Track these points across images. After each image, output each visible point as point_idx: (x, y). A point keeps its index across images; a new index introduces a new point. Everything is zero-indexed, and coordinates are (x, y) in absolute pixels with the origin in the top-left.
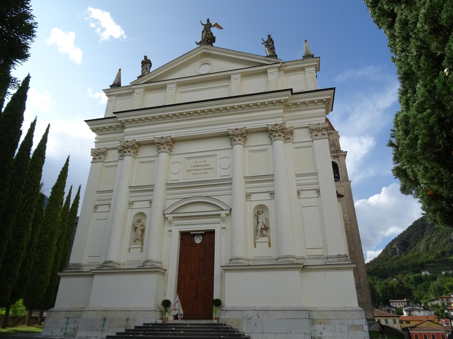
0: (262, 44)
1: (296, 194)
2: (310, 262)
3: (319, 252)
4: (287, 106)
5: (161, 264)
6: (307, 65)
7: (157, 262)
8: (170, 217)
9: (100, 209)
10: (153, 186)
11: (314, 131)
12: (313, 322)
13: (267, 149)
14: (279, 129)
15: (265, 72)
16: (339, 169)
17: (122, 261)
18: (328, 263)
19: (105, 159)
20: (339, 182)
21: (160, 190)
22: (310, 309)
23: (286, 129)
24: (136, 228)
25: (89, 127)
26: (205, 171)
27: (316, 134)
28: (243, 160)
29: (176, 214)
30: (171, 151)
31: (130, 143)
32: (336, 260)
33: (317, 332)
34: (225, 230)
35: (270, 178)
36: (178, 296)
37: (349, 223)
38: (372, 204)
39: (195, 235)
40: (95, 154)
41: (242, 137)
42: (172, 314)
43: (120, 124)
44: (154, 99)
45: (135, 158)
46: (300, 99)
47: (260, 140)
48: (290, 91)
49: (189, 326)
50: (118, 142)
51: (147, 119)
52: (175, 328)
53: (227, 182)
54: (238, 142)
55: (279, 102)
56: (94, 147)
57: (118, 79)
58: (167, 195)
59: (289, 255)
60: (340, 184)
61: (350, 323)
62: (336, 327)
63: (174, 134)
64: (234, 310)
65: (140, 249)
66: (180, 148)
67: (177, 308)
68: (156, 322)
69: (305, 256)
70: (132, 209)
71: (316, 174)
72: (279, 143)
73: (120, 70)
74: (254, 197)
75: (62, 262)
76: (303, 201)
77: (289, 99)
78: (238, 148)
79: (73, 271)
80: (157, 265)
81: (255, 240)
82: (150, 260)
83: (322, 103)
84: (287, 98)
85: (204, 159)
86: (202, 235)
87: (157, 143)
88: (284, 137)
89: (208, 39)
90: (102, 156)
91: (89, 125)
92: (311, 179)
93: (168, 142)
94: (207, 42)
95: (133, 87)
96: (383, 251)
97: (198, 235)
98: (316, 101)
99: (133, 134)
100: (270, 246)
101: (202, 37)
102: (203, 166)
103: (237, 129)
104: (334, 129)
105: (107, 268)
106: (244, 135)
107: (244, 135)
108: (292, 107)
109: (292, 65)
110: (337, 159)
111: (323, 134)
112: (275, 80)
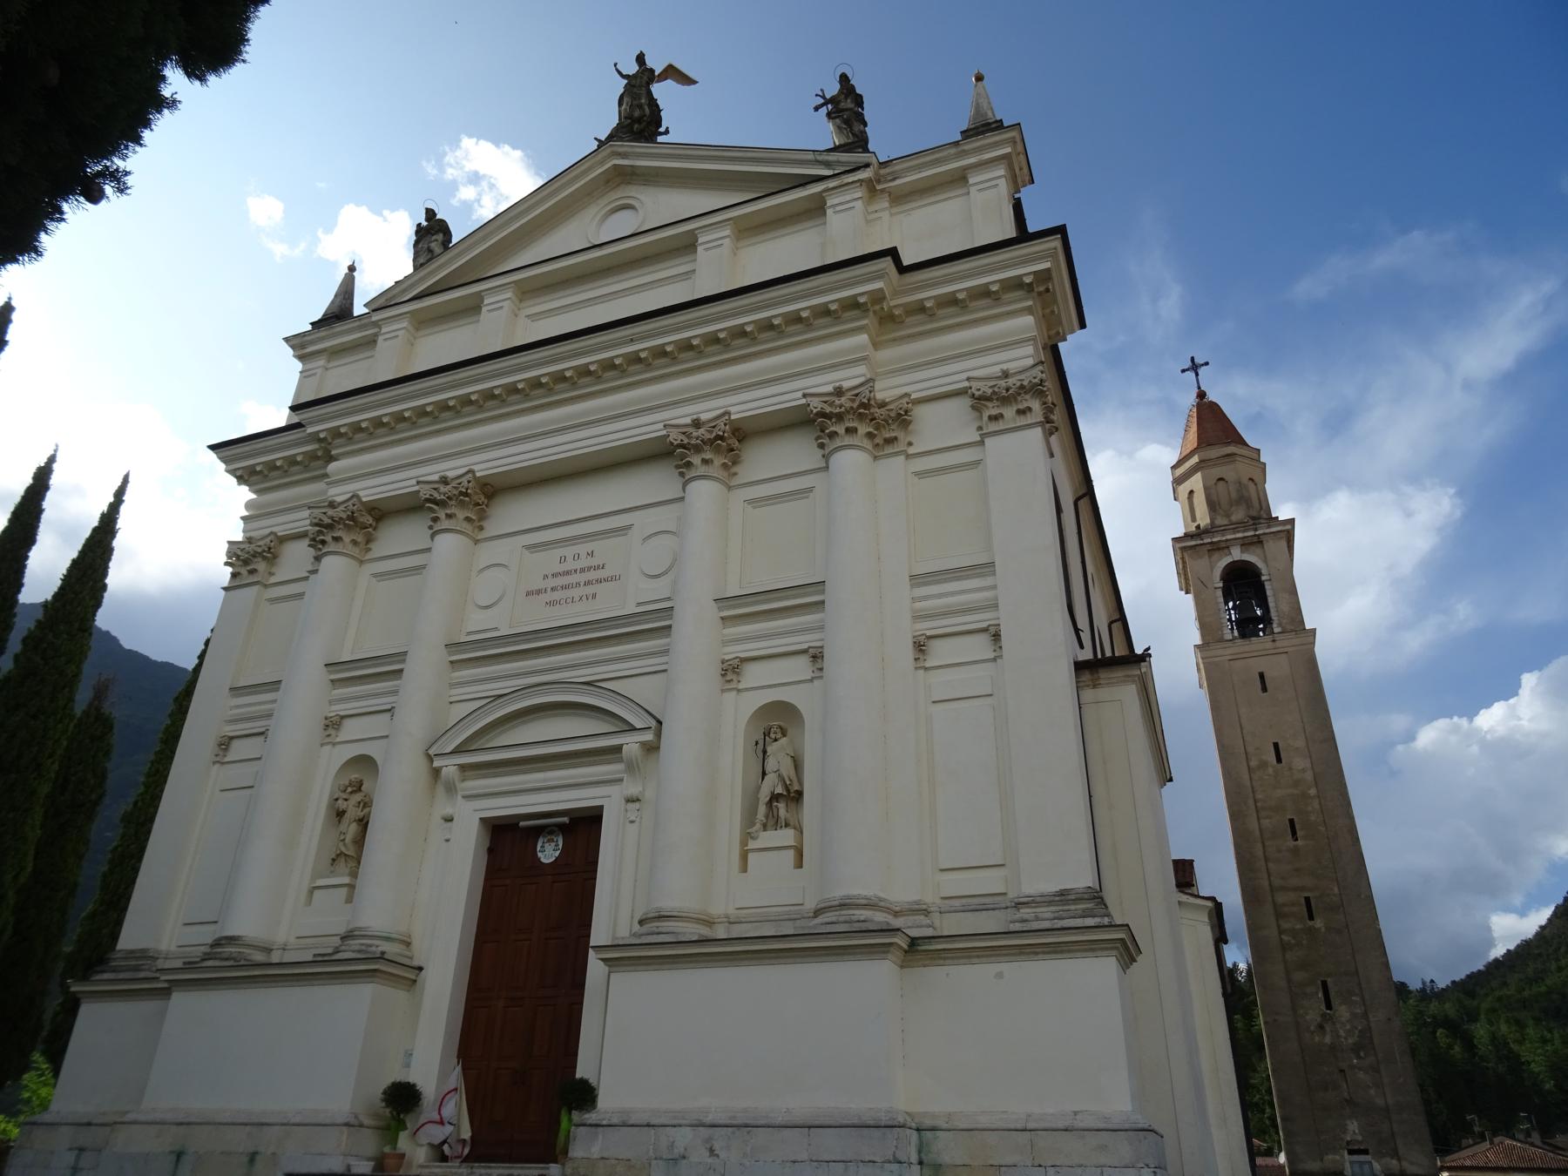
0: (817, 109)
1: (909, 652)
2: (949, 925)
3: (988, 883)
4: (888, 320)
6: (972, 160)
7: (388, 939)
8: (449, 767)
9: (941, 652)
10: (401, 656)
11: (991, 402)
13: (811, 489)
14: (848, 405)
16: (1268, 586)
17: (282, 935)
18: (1013, 927)
19: (271, 574)
20: (1269, 638)
21: (425, 669)
22: (928, 1123)
23: (883, 405)
24: (340, 814)
25: (223, 466)
26: (590, 590)
27: (994, 412)
29: (474, 753)
30: (481, 528)
31: (342, 508)
32: (1046, 911)
34: (637, 805)
35: (807, 598)
36: (459, 1068)
37: (1313, 792)
39: (538, 831)
40: (238, 557)
41: (718, 450)
42: (424, 1141)
45: (361, 562)
46: (931, 287)
47: (786, 456)
48: (906, 263)
50: (306, 513)
51: (400, 418)
53: (654, 624)
54: (702, 470)
55: (853, 304)
56: (239, 537)
58: (452, 686)
59: (854, 897)
60: (1269, 645)
63: (486, 465)
64: (625, 1125)
65: (344, 891)
68: (349, 1167)
69: (930, 898)
70: (334, 744)
71: (987, 568)
72: (851, 461)
74: (754, 675)
75: (97, 949)
76: (936, 677)
77: (891, 295)
78: (704, 492)
79: (122, 976)
80: (391, 949)
81: (744, 843)
82: (360, 929)
84: (878, 285)
85: (589, 547)
86: (562, 828)
87: (428, 500)
89: (639, 118)
90: (261, 566)
91: (223, 459)
93: (466, 494)
94: (632, 132)
96: (1555, 914)
97: (551, 833)
98: (994, 288)
99: (363, 476)
100: (799, 864)
102: (582, 570)
103: (697, 424)
105: (228, 965)
106: (729, 442)
107: (729, 442)
108: (909, 320)
109: (920, 167)
110: (1259, 551)
111: (1021, 412)
112: (850, 226)
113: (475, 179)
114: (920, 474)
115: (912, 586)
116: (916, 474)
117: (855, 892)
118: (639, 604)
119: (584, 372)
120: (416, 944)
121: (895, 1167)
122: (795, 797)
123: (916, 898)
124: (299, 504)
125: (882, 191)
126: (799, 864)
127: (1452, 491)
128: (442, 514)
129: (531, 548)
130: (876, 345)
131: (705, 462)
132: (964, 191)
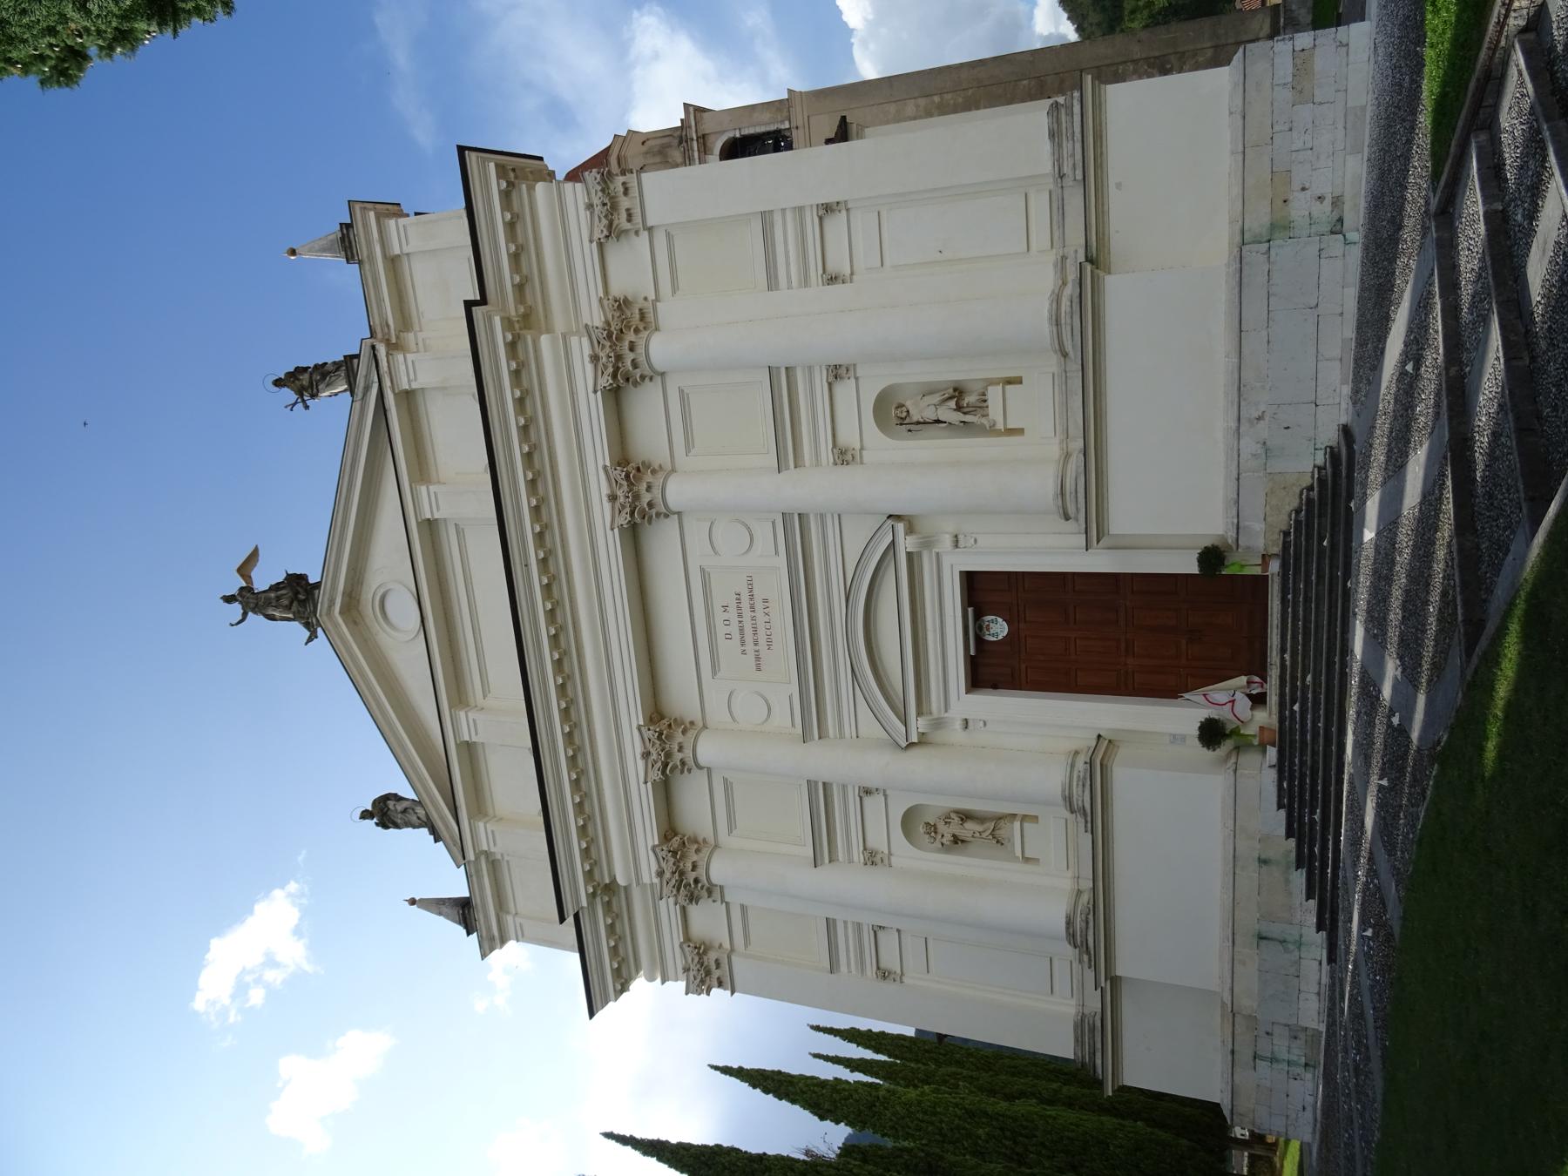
0: (307, 407)
1: (837, 288)
2: (1076, 238)
4: (527, 319)
5: (1077, 753)
7: (1072, 766)
8: (918, 725)
10: (811, 785)
11: (614, 222)
12: (1280, 228)
13: (681, 391)
14: (608, 350)
15: (409, 398)
16: (746, 132)
17: (1066, 884)
18: (1079, 177)
20: (794, 132)
21: (825, 761)
22: (1238, 239)
23: (608, 323)
24: (956, 840)
26: (759, 606)
27: (624, 215)
28: (721, 476)
30: (692, 723)
31: (664, 865)
32: (1067, 146)
33: (1315, 214)
34: (961, 537)
35: (782, 381)
36: (1187, 696)
37: (936, 99)
38: (871, 17)
39: (980, 640)
40: (702, 982)
41: (638, 479)
43: (598, 900)
44: (511, 783)
49: (1287, 657)
52: (1293, 702)
53: (797, 529)
54: (657, 492)
55: (512, 347)
56: (682, 985)
57: (444, 909)
58: (842, 736)
59: (1050, 312)
60: (801, 131)
61: (1287, 94)
62: (1299, 145)
63: (632, 714)
64: (1238, 502)
66: (681, 694)
67: (1226, 698)
69: (1051, 257)
70: (890, 854)
71: (766, 218)
72: (660, 349)
73: (413, 902)
74: (848, 436)
75: (1071, 1082)
76: (860, 265)
77: (502, 311)
78: (677, 492)
79: (1099, 1045)
80: (1081, 765)
81: (998, 433)
82: (1063, 791)
83: (514, 195)
84: (497, 320)
85: (718, 610)
86: (978, 616)
87: (664, 772)
88: (637, 331)
89: (296, 598)
90: (712, 957)
92: (786, 235)
93: (661, 734)
95: (471, 856)
97: (981, 628)
99: (633, 854)
101: (289, 619)
102: (740, 615)
103: (613, 498)
104: (606, 152)
105: (1092, 932)
107: (630, 471)
109: (380, 301)
110: (711, 139)
112: (436, 362)
113: (241, 989)
114: (675, 288)
115: (777, 289)
116: (674, 292)
117: (1046, 314)
118: (777, 553)
119: (551, 615)
120: (1074, 746)
121: (1273, 252)
122: (958, 392)
123: (1051, 268)
124: (656, 918)
125: (397, 337)
126: (1018, 381)
127: (636, 14)
128: (678, 756)
129: (715, 669)
130: (549, 330)
131: (649, 489)
132: (405, 260)
